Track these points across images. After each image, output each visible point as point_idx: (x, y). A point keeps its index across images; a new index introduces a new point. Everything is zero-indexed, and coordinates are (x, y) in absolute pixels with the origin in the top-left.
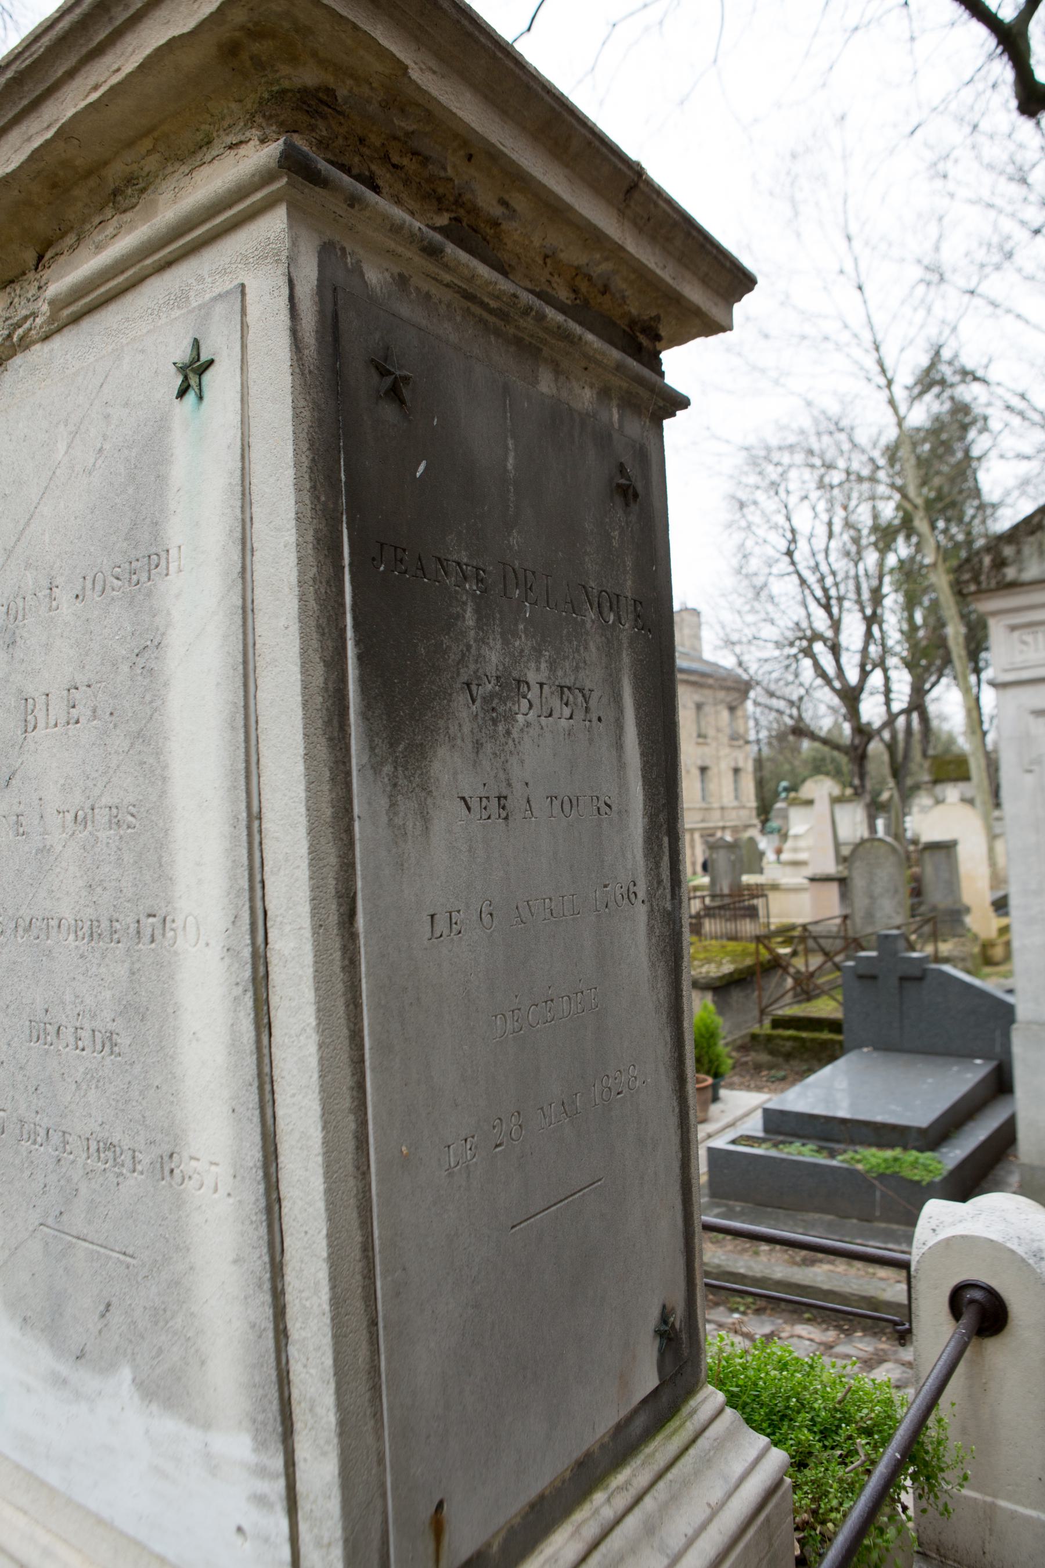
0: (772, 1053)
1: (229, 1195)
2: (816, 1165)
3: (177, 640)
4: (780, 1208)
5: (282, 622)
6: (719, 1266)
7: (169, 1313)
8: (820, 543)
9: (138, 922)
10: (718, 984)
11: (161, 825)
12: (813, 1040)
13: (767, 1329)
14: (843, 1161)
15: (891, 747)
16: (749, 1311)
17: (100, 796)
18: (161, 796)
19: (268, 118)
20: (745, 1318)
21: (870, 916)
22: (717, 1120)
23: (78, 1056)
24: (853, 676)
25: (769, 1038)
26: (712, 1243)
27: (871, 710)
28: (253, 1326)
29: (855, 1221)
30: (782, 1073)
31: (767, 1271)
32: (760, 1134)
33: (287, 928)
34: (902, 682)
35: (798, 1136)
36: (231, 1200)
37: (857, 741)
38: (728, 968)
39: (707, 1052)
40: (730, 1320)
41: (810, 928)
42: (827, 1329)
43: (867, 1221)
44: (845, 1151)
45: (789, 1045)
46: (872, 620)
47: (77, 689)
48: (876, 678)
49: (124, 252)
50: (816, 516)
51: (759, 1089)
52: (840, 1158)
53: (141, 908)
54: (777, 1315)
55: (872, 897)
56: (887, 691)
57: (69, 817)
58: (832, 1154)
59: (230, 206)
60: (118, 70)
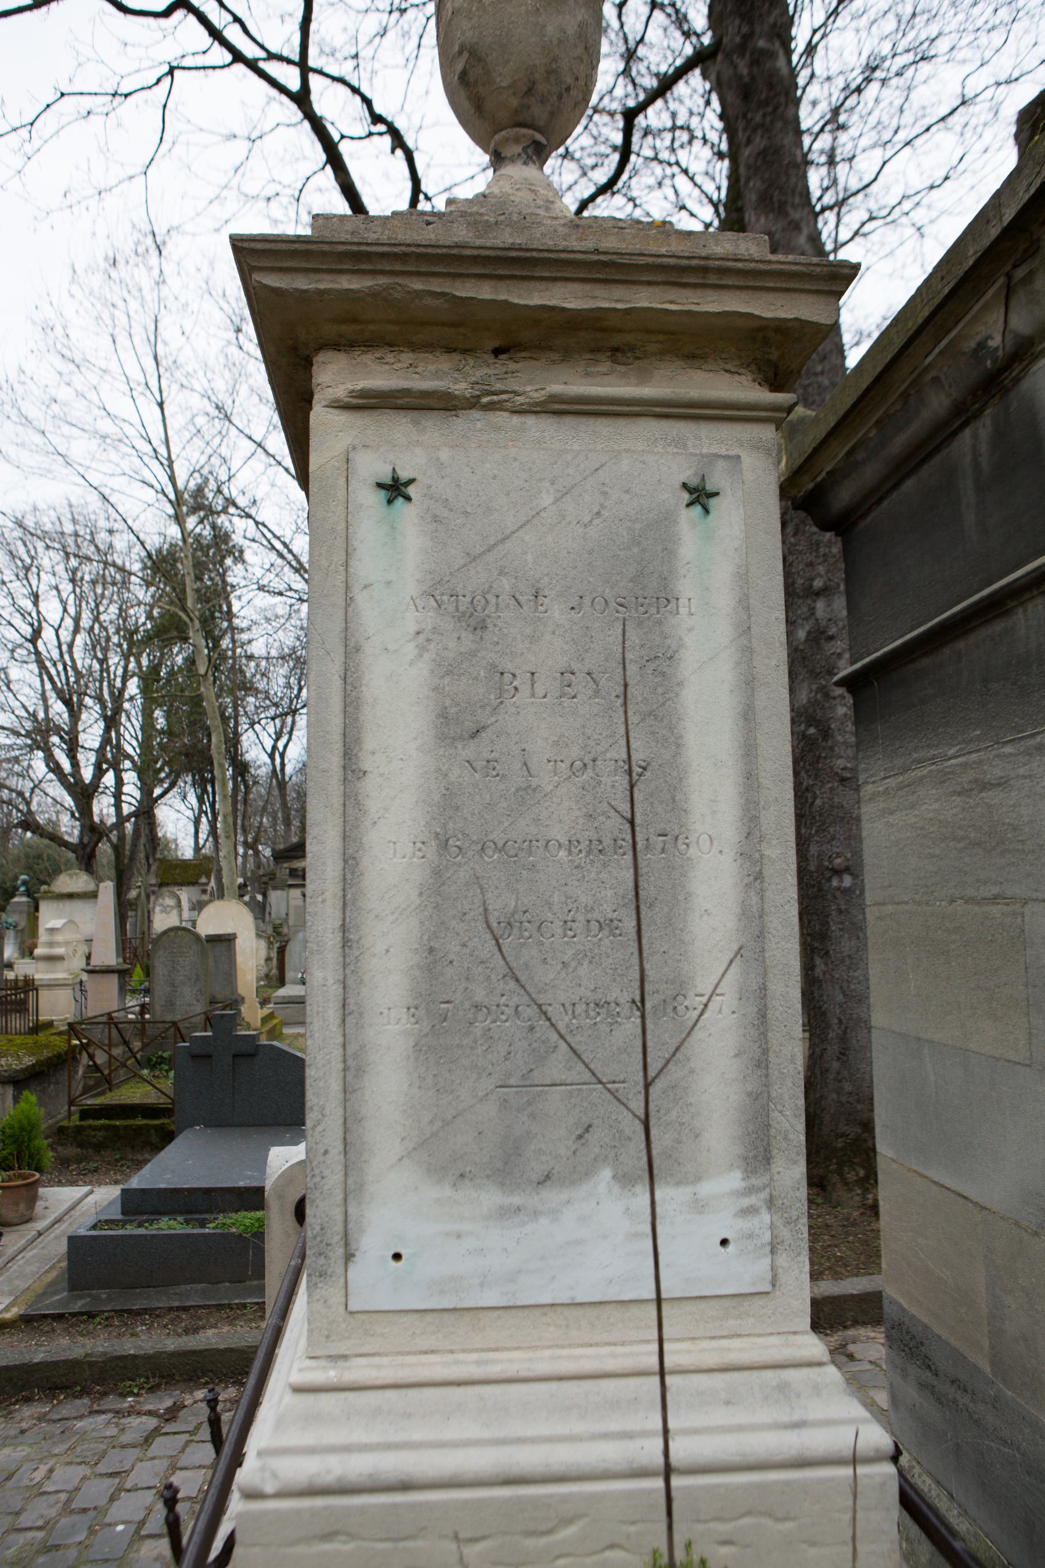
0: (80, 1145)
1: (734, 1012)
2: (188, 1235)
3: (690, 658)
4: (149, 1287)
5: (774, 662)
6: (105, 1354)
7: (662, 1112)
8: (65, 636)
9: (647, 840)
10: (22, 1077)
11: (675, 774)
12: (125, 1127)
13: (168, 1403)
14: (216, 1228)
15: (117, 849)
16: (143, 1392)
17: (607, 750)
18: (674, 756)
19: (759, 369)
20: (141, 1399)
21: (170, 1004)
22: (44, 1217)
23: (567, 943)
24: (87, 774)
25: (79, 1130)
26: (83, 1335)
27: (103, 807)
28: (749, 1094)
29: (227, 1284)
30: (93, 1165)
31: (160, 1346)
32: (120, 1217)
33: (774, 842)
34: (132, 789)
35: (165, 1214)
36: (735, 1016)
37: (86, 840)
38: (28, 1061)
39: (27, 1147)
40: (127, 1405)
41: (113, 1015)
42: (227, 1387)
43: (240, 1282)
44: (216, 1219)
45: (100, 1134)
46: (111, 722)
47: (573, 674)
48: (109, 779)
49: (627, 396)
50: (65, 610)
51: (73, 1183)
52: (211, 1225)
53: (652, 830)
54: (172, 1388)
55: (173, 985)
56: (118, 795)
57: (563, 767)
58: (203, 1224)
59: (739, 409)
60: (698, 304)
